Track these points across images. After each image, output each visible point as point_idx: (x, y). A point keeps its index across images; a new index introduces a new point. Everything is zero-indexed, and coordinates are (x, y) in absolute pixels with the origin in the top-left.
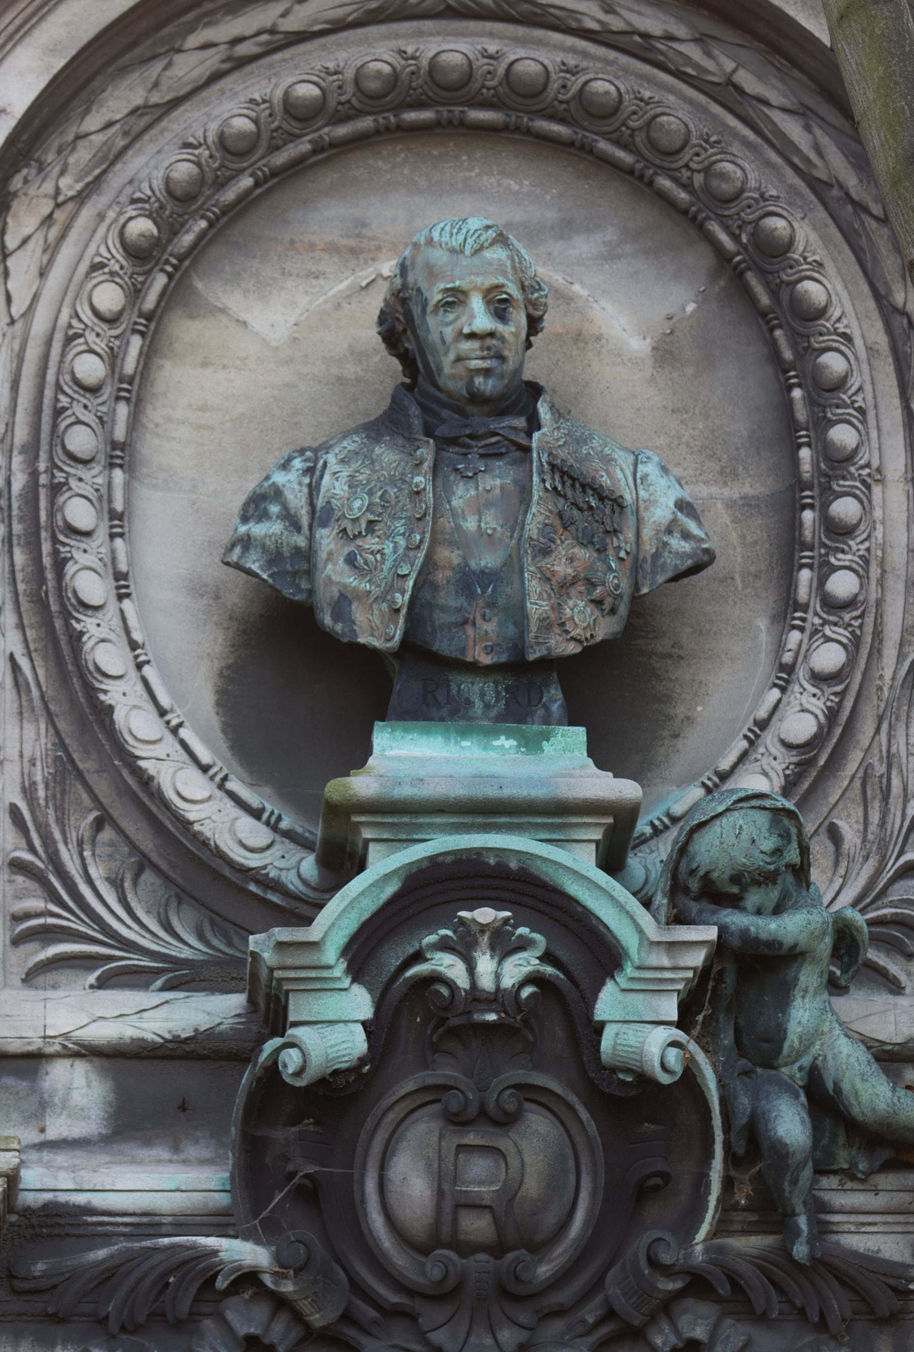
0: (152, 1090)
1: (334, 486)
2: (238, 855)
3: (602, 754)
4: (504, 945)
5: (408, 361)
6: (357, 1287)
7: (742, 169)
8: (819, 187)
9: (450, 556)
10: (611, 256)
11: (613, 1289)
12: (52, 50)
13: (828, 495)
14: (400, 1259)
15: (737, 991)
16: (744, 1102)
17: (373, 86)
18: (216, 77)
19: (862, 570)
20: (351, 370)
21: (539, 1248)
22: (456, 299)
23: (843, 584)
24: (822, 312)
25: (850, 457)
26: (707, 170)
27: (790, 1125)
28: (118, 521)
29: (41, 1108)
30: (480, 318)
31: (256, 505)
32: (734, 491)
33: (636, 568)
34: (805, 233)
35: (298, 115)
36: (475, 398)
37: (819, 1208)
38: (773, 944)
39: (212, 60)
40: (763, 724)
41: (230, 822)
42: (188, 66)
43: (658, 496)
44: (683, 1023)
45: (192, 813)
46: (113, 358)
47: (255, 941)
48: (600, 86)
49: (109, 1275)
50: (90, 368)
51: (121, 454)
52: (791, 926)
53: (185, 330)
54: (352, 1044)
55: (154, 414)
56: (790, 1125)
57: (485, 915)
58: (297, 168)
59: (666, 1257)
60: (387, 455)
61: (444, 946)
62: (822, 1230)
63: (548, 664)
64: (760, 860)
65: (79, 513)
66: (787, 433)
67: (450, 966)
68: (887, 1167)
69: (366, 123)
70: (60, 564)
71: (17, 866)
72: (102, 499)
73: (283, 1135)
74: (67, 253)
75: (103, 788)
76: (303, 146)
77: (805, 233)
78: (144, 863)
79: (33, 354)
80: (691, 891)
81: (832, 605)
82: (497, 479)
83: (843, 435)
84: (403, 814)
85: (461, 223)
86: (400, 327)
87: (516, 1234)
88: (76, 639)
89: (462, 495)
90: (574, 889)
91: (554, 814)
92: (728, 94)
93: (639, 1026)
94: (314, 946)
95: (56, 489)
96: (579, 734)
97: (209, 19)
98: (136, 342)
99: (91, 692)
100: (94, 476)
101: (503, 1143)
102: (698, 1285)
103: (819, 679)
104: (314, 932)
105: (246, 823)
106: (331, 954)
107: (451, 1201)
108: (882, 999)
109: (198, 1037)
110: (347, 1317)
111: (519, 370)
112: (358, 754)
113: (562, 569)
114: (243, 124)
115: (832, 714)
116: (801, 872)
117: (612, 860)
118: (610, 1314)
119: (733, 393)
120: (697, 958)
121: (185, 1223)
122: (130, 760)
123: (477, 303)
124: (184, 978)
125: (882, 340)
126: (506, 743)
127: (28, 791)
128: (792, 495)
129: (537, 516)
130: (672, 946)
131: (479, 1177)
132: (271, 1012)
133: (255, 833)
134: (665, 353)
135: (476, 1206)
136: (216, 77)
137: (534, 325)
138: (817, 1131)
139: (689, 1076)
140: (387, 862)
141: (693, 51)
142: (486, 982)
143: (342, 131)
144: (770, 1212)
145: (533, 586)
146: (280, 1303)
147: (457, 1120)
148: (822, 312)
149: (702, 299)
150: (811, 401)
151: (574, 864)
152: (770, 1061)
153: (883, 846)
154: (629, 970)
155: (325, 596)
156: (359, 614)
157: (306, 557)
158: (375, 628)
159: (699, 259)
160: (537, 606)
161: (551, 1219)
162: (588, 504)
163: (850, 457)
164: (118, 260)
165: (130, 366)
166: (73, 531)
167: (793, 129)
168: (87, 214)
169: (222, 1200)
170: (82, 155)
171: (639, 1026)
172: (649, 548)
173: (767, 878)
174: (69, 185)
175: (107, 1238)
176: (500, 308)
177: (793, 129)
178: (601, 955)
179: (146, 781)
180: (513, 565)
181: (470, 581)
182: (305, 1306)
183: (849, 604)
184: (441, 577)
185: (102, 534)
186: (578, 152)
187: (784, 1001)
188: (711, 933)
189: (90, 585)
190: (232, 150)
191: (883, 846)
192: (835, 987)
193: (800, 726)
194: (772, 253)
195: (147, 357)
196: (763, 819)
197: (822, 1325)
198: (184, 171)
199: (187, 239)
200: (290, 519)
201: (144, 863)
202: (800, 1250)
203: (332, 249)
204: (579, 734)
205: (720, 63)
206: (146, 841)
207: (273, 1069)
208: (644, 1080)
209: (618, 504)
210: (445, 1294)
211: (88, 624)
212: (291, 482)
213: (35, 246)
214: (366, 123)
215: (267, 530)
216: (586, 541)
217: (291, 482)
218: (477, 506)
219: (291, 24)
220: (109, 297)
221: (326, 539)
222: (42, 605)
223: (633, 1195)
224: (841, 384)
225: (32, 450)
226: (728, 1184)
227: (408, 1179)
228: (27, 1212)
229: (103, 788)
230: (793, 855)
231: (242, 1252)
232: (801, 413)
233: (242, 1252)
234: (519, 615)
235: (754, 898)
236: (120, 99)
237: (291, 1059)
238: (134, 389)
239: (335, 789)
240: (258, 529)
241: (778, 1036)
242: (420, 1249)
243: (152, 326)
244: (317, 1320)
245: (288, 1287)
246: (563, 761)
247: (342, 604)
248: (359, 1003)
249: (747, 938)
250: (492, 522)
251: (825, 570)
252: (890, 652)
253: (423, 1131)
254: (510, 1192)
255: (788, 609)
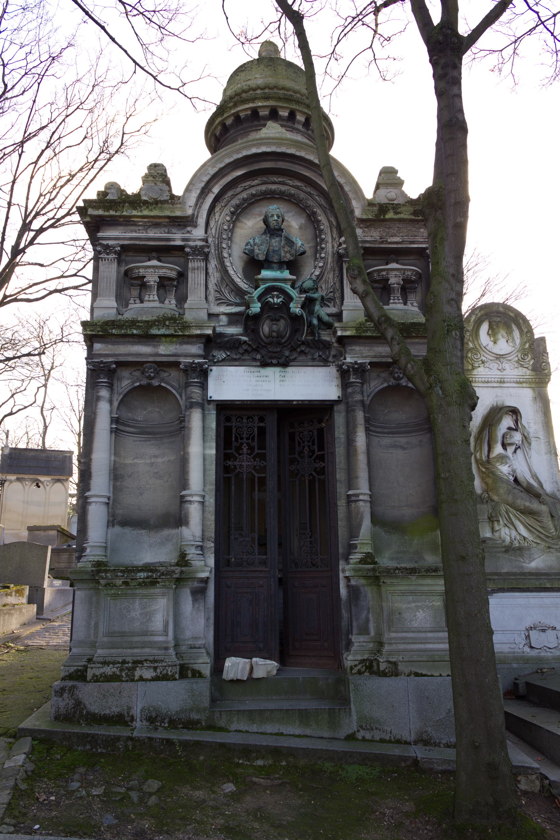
0: (233, 319)
1: (257, 241)
2: (244, 289)
3: (291, 273)
4: (278, 297)
5: (266, 225)
6: (259, 343)
7: (310, 202)
8: (320, 205)
9: (271, 248)
10: (294, 215)
11: (292, 343)
12: (221, 185)
13: (321, 244)
14: (265, 339)
15: (308, 304)
16: (309, 319)
17: (263, 192)
18: (242, 191)
19: (325, 253)
20: (260, 230)
21: (283, 338)
22: (272, 216)
23: (323, 255)
24: (321, 221)
25: (324, 239)
26: (306, 203)
27: (315, 322)
28: (230, 247)
29: (219, 321)
30: (276, 218)
31: (247, 245)
32: (309, 245)
33: (296, 251)
34: (319, 211)
35: (253, 196)
36: (275, 229)
37: (319, 334)
38: (313, 298)
39: (242, 189)
40: (312, 273)
41: (243, 285)
42: (239, 189)
43: (299, 243)
44: (301, 308)
45: (239, 284)
46: (229, 226)
47: (246, 297)
48: (292, 192)
49: (227, 342)
50: (226, 227)
51: (230, 239)
52: (315, 295)
53: (238, 224)
54: (258, 310)
55: (234, 235)
56: (315, 322)
57: (275, 293)
58: (253, 203)
59: (299, 339)
60: (264, 236)
61: (270, 297)
62: (319, 336)
63: (284, 262)
64: (311, 287)
65: (224, 246)
66: (316, 237)
67: (271, 300)
68: (328, 328)
69: (262, 197)
70: (222, 252)
71: (216, 291)
72: (227, 244)
73: (250, 323)
74: (223, 213)
75: (227, 281)
76: (254, 200)
77: (319, 211)
78: (232, 291)
79: (218, 226)
80: (303, 291)
81: (322, 258)
82: (278, 239)
83: (323, 236)
84: (265, 280)
85: (274, 209)
86: (265, 221)
87: (280, 336)
88: (224, 261)
89: (273, 241)
90: (287, 290)
91: (285, 280)
92: (310, 194)
93: (295, 308)
94: (253, 297)
95: (221, 243)
96: (288, 271)
97: (241, 183)
98: (232, 225)
99: (226, 268)
100: (226, 241)
101: (278, 323)
102: (303, 343)
103: (320, 267)
104: (253, 295)
105: (245, 285)
106: (255, 298)
107: (271, 331)
108: (327, 308)
109: (239, 312)
110: (258, 347)
111: (281, 226)
112: (260, 273)
113: (286, 250)
114: (246, 196)
115: (321, 272)
116: (317, 289)
117: (293, 286)
118: (292, 347)
119: (309, 233)
120: (303, 299)
121: (237, 335)
122: (231, 277)
123: (275, 216)
124: (237, 305)
125: (328, 225)
126: (279, 272)
127: (218, 281)
128: (317, 244)
129: (283, 243)
130: (300, 297)
131: (275, 328)
132: (248, 307)
133: (247, 286)
134: (300, 228)
135: (274, 331)
136: (242, 191)
137: (283, 221)
138: (319, 323)
139: (302, 315)
140: (262, 287)
141: (304, 188)
142: (276, 302)
143: (259, 198)
144: (312, 333)
145: (282, 252)
146: (249, 345)
147: (272, 320)
148: (321, 221)
149: (305, 221)
150: (319, 233)
151: (287, 287)
152: (313, 314)
153: (328, 289)
154: (356, 644)
155: (255, 254)
156: (260, 256)
157: (253, 250)
158: (261, 258)
159: (305, 215)
160: (283, 254)
161: (284, 334)
162: (290, 242)
163: (324, 239)
164: (229, 214)
165: (231, 228)
166: (223, 248)
167: (317, 198)
168: (225, 209)
169: (242, 332)
170: (225, 201)
171: (295, 308)
172: (298, 249)
173: (312, 289)
174: (223, 204)
175: (227, 337)
176: (278, 217)
177: (317, 198)
178: (291, 299)
179: (233, 280)
180: (280, 249)
181: (274, 251)
182: (252, 345)
183: (324, 258)
184: (270, 251)
185: (227, 249)
186: (289, 201)
187: (315, 305)
188: (305, 296)
189: (225, 255)
190: (244, 200)
191: (328, 289)
192: (322, 307)
193: (317, 273)
194: (314, 213)
195: (234, 227)
196: (312, 281)
197: (319, 348)
198: (238, 202)
199: (238, 212)
200: (251, 246)
201: (232, 291)
202: (316, 338)
203: (258, 215)
204: (288, 271)
205: (308, 190)
206: (233, 288)
207: (248, 314)
208: (296, 315)
209: (294, 243)
210: (271, 343)
211: (225, 260)
212: (251, 241)
213: (219, 212)
214: (262, 197)
215: (249, 247)
216: (289, 247)
217: (251, 241)
218: (275, 242)
219: (252, 184)
220: (228, 218)
221: (256, 247)
222: (219, 258)
223: (295, 331)
224: (323, 230)
225: (218, 238)
226: (307, 330)
227: (266, 328)
228: (217, 334)
229: (227, 281)
230: (316, 286)
231: (244, 338)
232: (318, 234)
233: (244, 338)
234: (280, 255)
235: (311, 292)
236: (230, 193)
237: (250, 312)
238: (232, 231)
239: (256, 277)
240: (247, 247)
241: (314, 310)
242: (267, 337)
243: (234, 223)
244: (254, 347)
245: (250, 343)
246: (286, 274)
247: (257, 255)
248: (259, 305)
249: (310, 297)
250: (277, 244)
251: (321, 254)
252: (329, 265)
253: (268, 322)
254: (279, 330)
255: (316, 259)
